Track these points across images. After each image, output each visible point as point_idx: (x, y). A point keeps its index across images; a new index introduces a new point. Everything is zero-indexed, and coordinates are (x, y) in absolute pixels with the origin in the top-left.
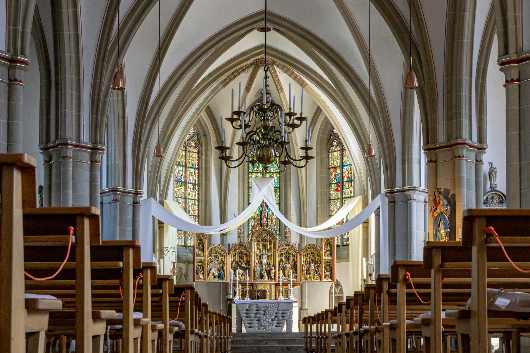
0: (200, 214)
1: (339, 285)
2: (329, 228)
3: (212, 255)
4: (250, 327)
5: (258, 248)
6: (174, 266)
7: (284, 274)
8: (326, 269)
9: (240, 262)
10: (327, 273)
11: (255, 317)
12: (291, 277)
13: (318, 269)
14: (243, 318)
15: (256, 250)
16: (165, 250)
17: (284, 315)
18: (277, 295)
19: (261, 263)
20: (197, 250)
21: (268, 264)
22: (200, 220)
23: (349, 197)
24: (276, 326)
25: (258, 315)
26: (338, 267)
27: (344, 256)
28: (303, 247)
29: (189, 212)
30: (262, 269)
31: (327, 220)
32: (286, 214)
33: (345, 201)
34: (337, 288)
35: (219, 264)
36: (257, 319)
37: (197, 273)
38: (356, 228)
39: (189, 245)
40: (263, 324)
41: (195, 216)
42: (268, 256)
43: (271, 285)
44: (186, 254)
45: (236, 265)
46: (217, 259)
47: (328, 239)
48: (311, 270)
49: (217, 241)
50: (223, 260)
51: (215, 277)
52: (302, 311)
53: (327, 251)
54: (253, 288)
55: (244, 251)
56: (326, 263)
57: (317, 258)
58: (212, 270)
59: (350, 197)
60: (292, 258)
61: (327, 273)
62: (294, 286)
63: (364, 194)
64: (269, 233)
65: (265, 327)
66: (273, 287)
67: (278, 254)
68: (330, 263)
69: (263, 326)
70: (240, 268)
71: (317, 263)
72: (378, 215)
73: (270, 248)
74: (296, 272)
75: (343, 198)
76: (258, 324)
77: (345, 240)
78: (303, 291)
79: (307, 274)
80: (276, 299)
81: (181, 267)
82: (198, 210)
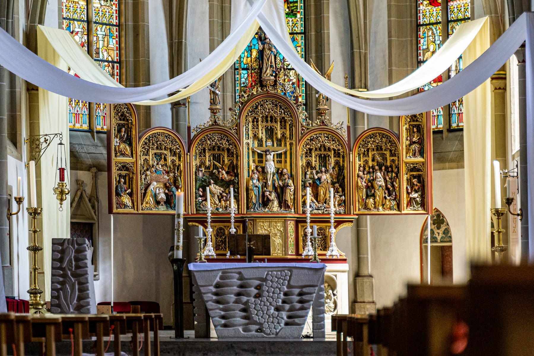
0: (123, 58)
2: (419, 91)
3: (151, 152)
4: (225, 326)
5: (255, 137)
6: (62, 179)
7: (316, 196)
8: (412, 185)
9: (215, 167)
11: (236, 302)
12: (332, 203)
13: (393, 186)
14: (210, 305)
15: (250, 141)
16: (42, 140)
17: (308, 292)
18: (301, 244)
19: (264, 171)
20: (115, 142)
21: (280, 173)
22: (124, 71)
23: (461, 20)
24: (287, 324)
25: (244, 299)
26: (439, 180)
27: (451, 155)
28: (359, 132)
29: (98, 53)
30: (265, 185)
31: (413, 71)
32: (321, 66)
33: (453, 28)
34: (439, 228)
35: (167, 173)
36: (242, 306)
38: (479, 89)
39: (99, 128)
40: (256, 318)
41: (113, 62)
43: (285, 220)
44: (92, 150)
45: (207, 175)
46: (162, 162)
47: (415, 116)
48: (377, 187)
49: (163, 119)
50: (177, 163)
51: (158, 203)
52: (359, 279)
53: (412, 143)
54: (245, 230)
55: (225, 144)
56: (412, 170)
57: (389, 158)
58: (151, 187)
59: (465, 19)
60: (332, 161)
61: (414, 195)
62: (338, 223)
63: (496, 12)
64: (281, 102)
65: (261, 324)
66: (291, 226)
67: (301, 150)
68: (419, 170)
69: (255, 323)
70: (216, 183)
71: (391, 170)
72: (522, 61)
73: (283, 135)
74: (343, 190)
75: (448, 22)
76: (245, 318)
77: (454, 118)
78: (362, 235)
79: (368, 196)
80: (298, 253)
82: (120, 49)
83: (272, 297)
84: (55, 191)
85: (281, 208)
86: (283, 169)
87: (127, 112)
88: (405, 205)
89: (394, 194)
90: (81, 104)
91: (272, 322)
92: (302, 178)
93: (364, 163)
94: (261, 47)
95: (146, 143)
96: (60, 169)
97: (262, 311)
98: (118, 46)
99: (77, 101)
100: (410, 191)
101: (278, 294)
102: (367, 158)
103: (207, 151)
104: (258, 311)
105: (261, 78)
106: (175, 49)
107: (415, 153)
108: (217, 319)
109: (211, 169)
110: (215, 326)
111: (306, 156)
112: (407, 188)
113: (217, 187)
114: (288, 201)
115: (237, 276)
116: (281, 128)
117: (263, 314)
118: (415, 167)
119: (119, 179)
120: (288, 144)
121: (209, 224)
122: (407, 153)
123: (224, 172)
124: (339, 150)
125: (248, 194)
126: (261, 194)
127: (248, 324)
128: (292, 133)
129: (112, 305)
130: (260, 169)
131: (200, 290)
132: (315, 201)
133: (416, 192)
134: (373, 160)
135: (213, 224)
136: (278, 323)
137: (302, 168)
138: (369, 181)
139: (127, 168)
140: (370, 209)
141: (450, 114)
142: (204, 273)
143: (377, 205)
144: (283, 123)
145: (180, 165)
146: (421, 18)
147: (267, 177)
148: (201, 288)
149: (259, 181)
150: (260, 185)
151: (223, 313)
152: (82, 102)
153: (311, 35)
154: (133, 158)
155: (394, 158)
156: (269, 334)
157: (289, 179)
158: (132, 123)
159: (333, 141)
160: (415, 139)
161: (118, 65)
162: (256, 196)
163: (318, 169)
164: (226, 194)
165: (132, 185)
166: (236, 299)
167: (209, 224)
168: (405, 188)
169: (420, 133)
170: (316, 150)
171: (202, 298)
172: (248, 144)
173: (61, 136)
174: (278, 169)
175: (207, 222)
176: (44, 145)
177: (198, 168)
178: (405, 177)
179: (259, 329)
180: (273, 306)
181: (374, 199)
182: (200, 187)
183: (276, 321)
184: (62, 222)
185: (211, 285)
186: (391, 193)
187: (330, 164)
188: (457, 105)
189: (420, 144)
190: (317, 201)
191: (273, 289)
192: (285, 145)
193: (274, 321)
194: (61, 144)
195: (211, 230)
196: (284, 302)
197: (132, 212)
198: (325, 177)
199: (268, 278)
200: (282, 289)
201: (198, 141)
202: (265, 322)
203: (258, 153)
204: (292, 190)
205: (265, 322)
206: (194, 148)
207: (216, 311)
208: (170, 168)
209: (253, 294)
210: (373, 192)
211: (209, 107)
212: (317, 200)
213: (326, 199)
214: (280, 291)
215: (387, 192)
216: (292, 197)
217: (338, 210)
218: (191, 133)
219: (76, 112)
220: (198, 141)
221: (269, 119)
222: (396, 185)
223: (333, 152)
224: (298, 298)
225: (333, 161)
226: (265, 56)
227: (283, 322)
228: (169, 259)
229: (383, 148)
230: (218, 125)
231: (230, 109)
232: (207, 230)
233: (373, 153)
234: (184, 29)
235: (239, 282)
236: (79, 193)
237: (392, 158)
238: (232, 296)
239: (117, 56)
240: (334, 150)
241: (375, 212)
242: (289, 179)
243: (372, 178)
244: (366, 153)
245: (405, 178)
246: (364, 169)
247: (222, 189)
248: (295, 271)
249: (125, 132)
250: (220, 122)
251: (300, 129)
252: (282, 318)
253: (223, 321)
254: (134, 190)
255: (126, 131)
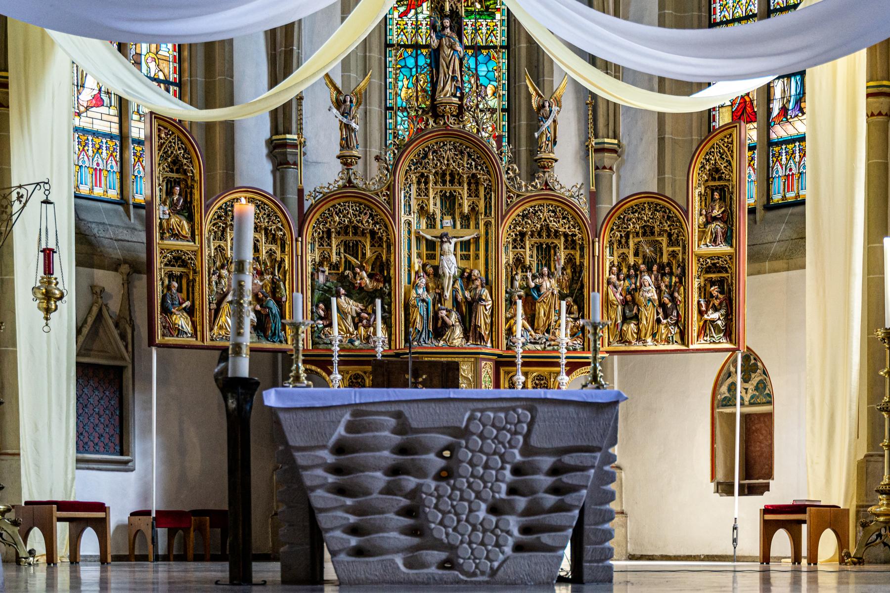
0: (186, 77)
1: (754, 368)
4: (359, 552)
6: (48, 269)
7: (531, 318)
9: (349, 266)
10: (713, 316)
11: (388, 490)
13: (673, 299)
14: (320, 498)
15: (413, 218)
16: (14, 196)
19: (437, 274)
21: (466, 278)
25: (411, 482)
26: (755, 290)
30: (439, 298)
36: (404, 502)
37: (166, 311)
40: (440, 533)
42: (465, 245)
44: (125, 235)
50: (278, 255)
53: (710, 220)
56: (708, 270)
60: (562, 255)
61: (713, 316)
62: (573, 367)
64: (470, 146)
65: (452, 548)
67: (505, 234)
68: (723, 269)
69: (438, 545)
70: (349, 295)
71: (671, 271)
73: (473, 209)
76: (412, 531)
79: (625, 319)
81: (102, 284)
83: (482, 478)
84: (34, 293)
85: (468, 341)
86: (471, 271)
87: (183, 157)
88: (695, 334)
89: (675, 313)
90: (104, 152)
91: (482, 543)
92: (507, 288)
93: (620, 260)
94: (435, 44)
95: (219, 217)
96: (44, 251)
97: (456, 514)
98: (176, 54)
99: (97, 146)
100: (704, 308)
101: (497, 471)
102: (625, 250)
103: (333, 235)
104: (444, 513)
105: (436, 100)
106: (280, 63)
107: (716, 237)
108: (338, 533)
109: (341, 269)
110: (333, 554)
111: (515, 247)
112: (699, 302)
113: (351, 302)
114: (480, 327)
115: (392, 422)
116: (470, 196)
117: (459, 521)
118: (714, 264)
119: (169, 281)
120: (482, 224)
121: (336, 365)
122: (700, 240)
123: (364, 274)
124: (575, 235)
125: (407, 315)
126: (431, 314)
127: (418, 548)
128: (490, 203)
129: (154, 515)
130: (429, 269)
131: (293, 460)
132: (530, 328)
133: (716, 310)
134: (636, 254)
135: (342, 367)
136: (497, 545)
137: (506, 269)
138: (629, 292)
139: (183, 261)
140: (630, 343)
141: (768, 178)
142: (302, 414)
143: (643, 334)
144: (473, 186)
145: (283, 260)
146: (718, 11)
147: (442, 284)
148: (298, 455)
149: (428, 291)
150: (430, 299)
151: (352, 519)
152: (107, 148)
153: (519, 48)
154: (194, 241)
155: (675, 249)
156: (474, 574)
157: (482, 287)
158: (193, 179)
159: (564, 218)
160: (716, 213)
161: (177, 89)
162: (422, 317)
163: (534, 271)
164: (369, 314)
165: (193, 293)
166: (389, 482)
167: (336, 365)
168: (695, 303)
169: (725, 201)
170: (532, 236)
171: (299, 480)
172: (409, 224)
173: (47, 187)
174: (463, 271)
175: (331, 363)
176: (17, 206)
177: (317, 267)
178: (695, 283)
179: (447, 561)
180: (484, 501)
181: (637, 325)
182: (319, 301)
183: (491, 539)
184: (58, 359)
185: (324, 447)
186: (669, 312)
187: (559, 259)
188: (784, 161)
189: (725, 222)
190: (533, 328)
191: (485, 458)
192: (477, 226)
193: (486, 541)
194: (47, 202)
195: (339, 377)
196: (512, 490)
197: (192, 343)
198: (548, 284)
199: (472, 428)
200: (508, 458)
201: (317, 215)
202: (462, 542)
203: (427, 240)
204: (488, 308)
205: (462, 542)
206: (310, 229)
207: (335, 518)
208: (266, 265)
209: (433, 472)
210: (635, 311)
211: (338, 152)
212: (532, 326)
213: (549, 325)
214: (504, 461)
215: (660, 311)
216: (488, 321)
217: (570, 344)
218: (305, 202)
219: (95, 166)
220: (317, 215)
221: (448, 178)
222: (680, 298)
223: (563, 239)
224: (549, 481)
225: (563, 257)
226: (442, 60)
227: (511, 541)
228: (216, 380)
229: (657, 229)
230: (354, 187)
231: (377, 158)
232: (332, 377)
233: (637, 240)
234: (296, 34)
235: (397, 439)
236: (95, 310)
237: (671, 249)
238: (379, 474)
239: (175, 72)
240: (566, 235)
241: (640, 347)
242: (482, 287)
243: (633, 286)
244: (623, 241)
245: (696, 285)
246: (620, 270)
247: (360, 306)
248: (542, 410)
249: (180, 194)
250: (358, 182)
251: (504, 196)
252: (508, 532)
253: (354, 541)
254: (197, 303)
255: (184, 194)
